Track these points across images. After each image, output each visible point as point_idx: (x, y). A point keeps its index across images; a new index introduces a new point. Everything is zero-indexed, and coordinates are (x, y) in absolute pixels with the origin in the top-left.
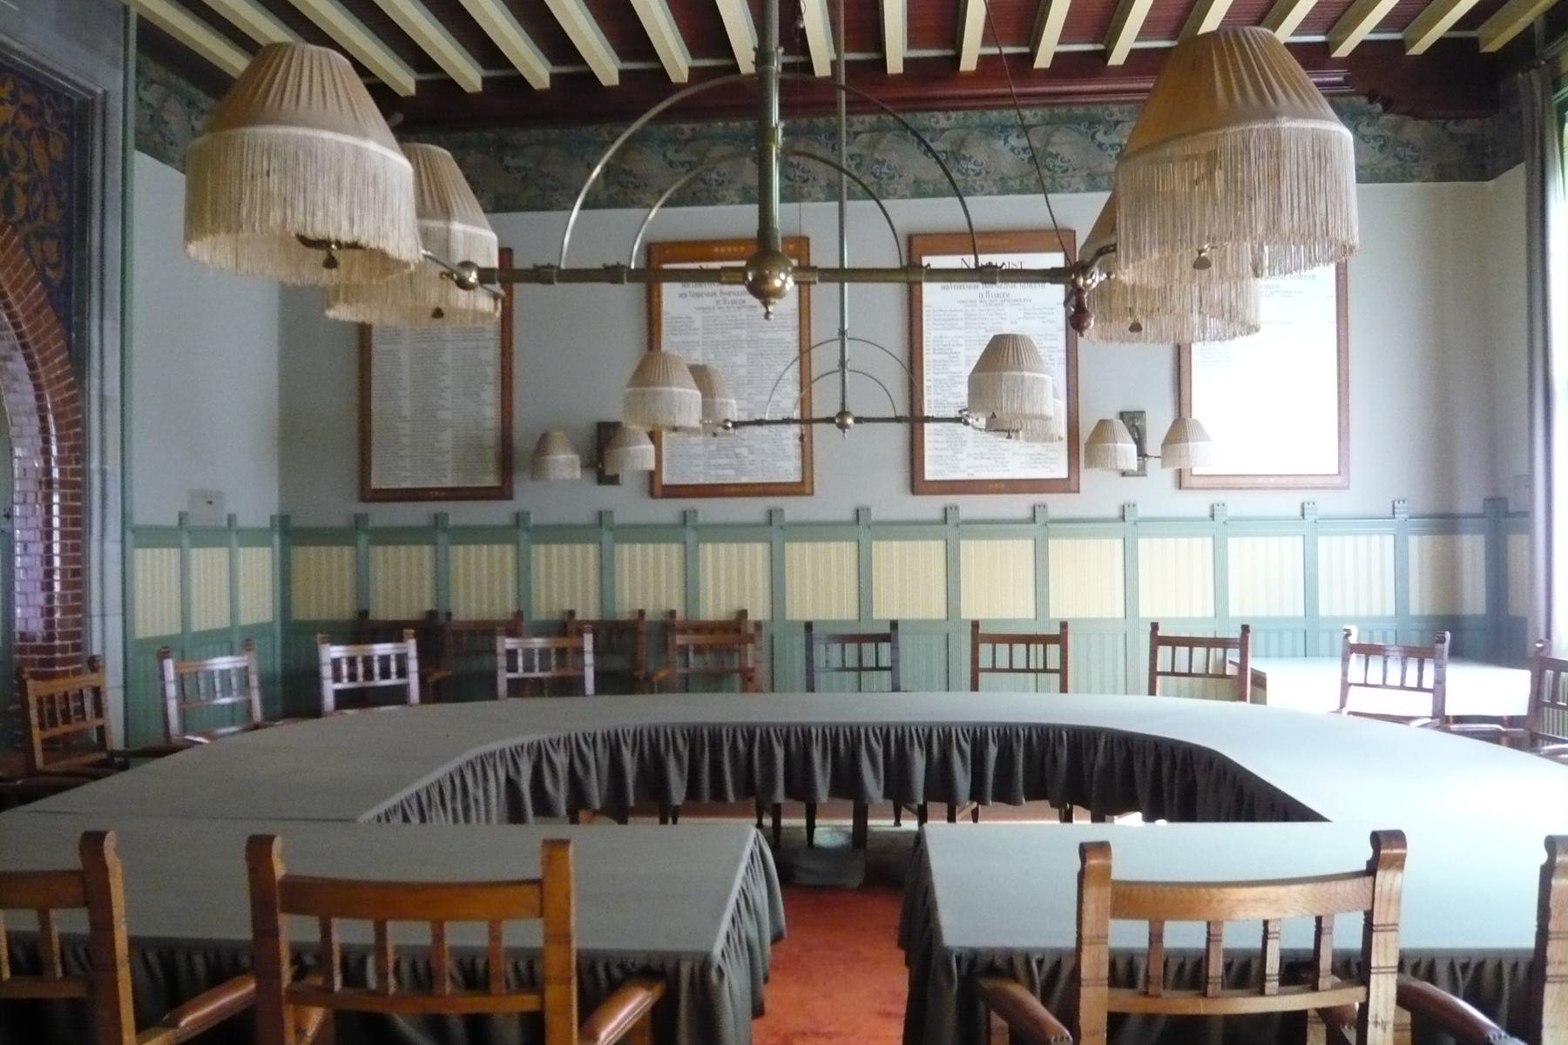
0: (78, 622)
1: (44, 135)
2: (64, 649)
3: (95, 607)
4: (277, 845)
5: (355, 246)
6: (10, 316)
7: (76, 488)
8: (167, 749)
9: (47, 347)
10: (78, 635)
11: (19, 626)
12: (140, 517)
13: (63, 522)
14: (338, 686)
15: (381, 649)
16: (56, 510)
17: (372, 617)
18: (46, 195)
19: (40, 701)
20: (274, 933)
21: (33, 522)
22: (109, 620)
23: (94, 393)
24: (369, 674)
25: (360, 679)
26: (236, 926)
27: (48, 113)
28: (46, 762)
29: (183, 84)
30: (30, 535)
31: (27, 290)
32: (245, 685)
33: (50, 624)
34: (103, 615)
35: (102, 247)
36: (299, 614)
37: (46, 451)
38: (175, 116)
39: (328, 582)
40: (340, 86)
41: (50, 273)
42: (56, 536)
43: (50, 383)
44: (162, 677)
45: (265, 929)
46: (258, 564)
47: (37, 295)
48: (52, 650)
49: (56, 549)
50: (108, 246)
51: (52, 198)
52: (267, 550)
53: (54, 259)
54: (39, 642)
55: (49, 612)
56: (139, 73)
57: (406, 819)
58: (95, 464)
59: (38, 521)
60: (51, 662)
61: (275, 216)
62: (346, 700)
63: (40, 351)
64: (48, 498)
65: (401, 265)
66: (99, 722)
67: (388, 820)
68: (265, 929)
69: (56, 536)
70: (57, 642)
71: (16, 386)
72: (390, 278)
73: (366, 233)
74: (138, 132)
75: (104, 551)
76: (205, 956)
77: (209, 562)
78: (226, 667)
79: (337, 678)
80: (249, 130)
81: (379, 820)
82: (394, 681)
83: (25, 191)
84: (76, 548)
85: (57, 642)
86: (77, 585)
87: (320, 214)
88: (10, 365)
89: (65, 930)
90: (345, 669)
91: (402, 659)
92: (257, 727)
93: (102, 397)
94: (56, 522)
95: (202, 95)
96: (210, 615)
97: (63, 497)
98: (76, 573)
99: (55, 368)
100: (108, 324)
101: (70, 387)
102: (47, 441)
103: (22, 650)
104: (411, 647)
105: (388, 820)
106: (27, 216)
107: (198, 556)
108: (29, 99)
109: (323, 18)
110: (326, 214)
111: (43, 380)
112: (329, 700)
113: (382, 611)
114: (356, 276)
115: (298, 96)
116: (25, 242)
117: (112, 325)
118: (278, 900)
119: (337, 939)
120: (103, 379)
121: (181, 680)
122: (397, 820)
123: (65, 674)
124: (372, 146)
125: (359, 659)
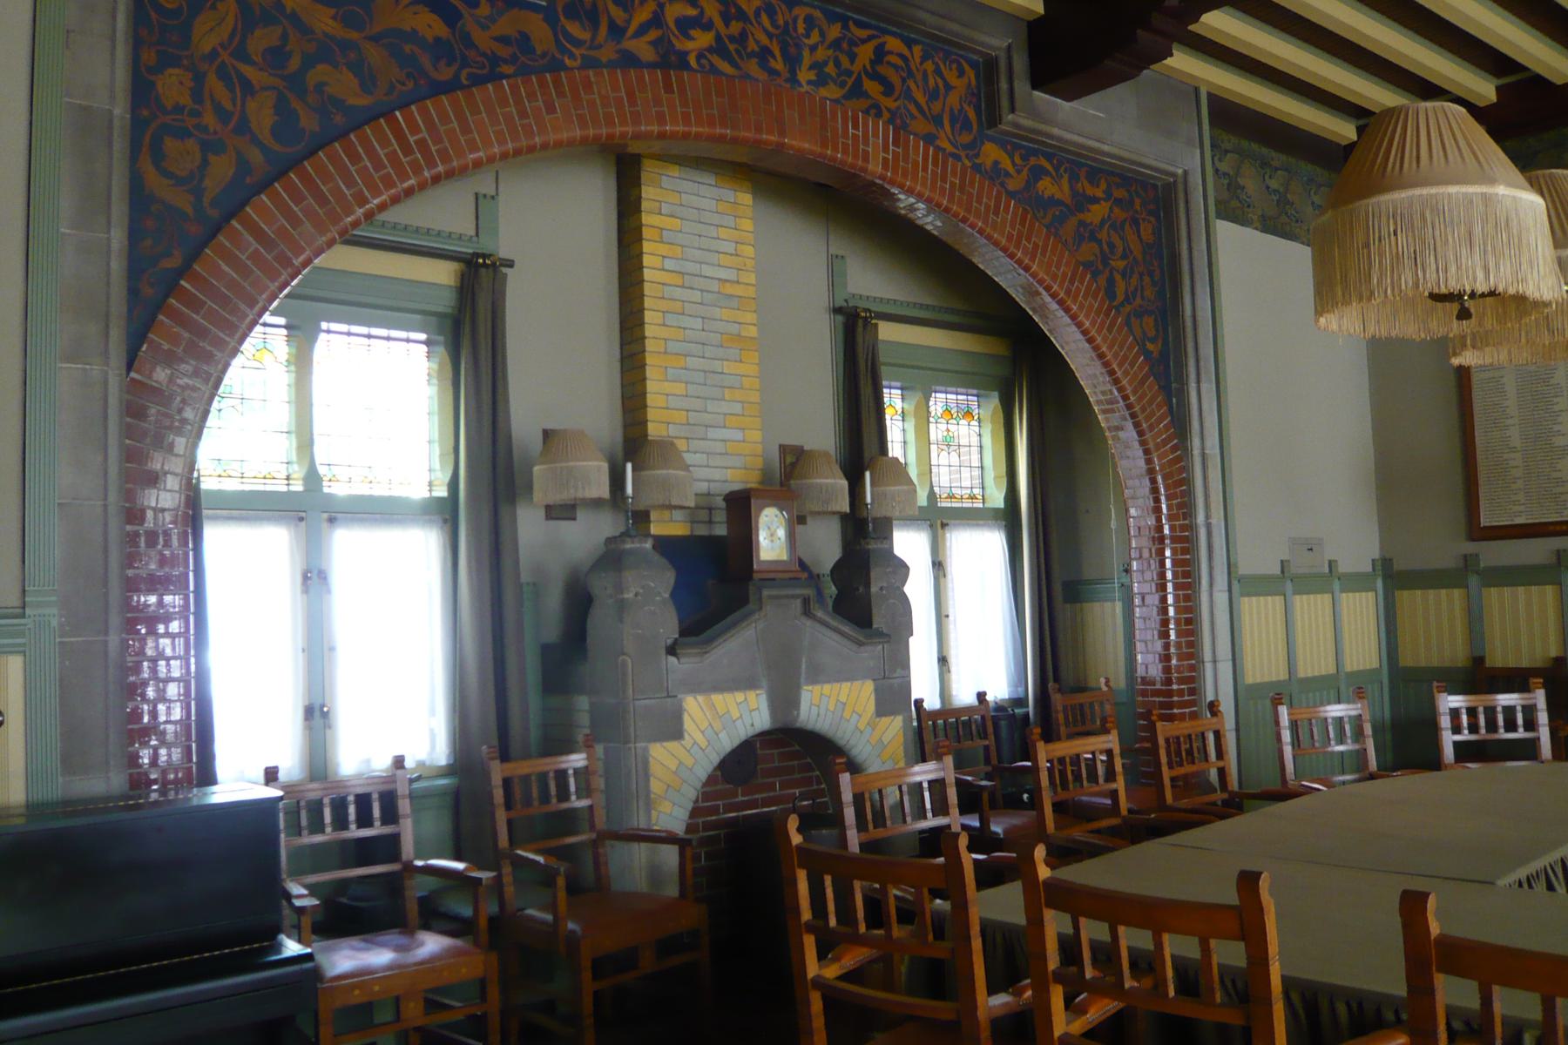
0: (1192, 668)
1: (1135, 222)
2: (1181, 693)
3: (1207, 656)
4: (1431, 903)
5: (1492, 294)
6: (1120, 390)
7: (1185, 542)
8: (1284, 794)
9: (1152, 414)
10: (1191, 680)
11: (1140, 671)
12: (1245, 568)
13: (1175, 575)
14: (1458, 738)
15: (1505, 699)
16: (1168, 563)
17: (1488, 664)
18: (1141, 275)
19: (1167, 741)
20: (1431, 992)
21: (1148, 575)
22: (1220, 666)
23: (1196, 452)
24: (1492, 726)
25: (1483, 731)
26: (1391, 982)
27: (1138, 202)
28: (1175, 799)
29: (1255, 146)
30: (1146, 588)
31: (1132, 365)
32: (1359, 734)
33: (1167, 670)
34: (1215, 661)
35: (1194, 317)
36: (1407, 660)
37: (1157, 510)
38: (1250, 183)
39: (1438, 625)
40: (1462, 143)
41: (1150, 346)
42: (1170, 587)
43: (1158, 447)
44: (1277, 723)
45: (1420, 987)
46: (1361, 610)
47: (1141, 368)
48: (1170, 693)
49: (1170, 599)
50: (1199, 314)
51: (1147, 279)
52: (1371, 595)
53: (1152, 333)
54: (1158, 686)
55: (1166, 658)
56: (1213, 146)
57: (1550, 887)
58: (1201, 518)
59: (1151, 574)
60: (1170, 706)
61: (1407, 279)
62: (1465, 752)
63: (1147, 419)
64: (1161, 553)
65: (1539, 305)
66: (1221, 764)
67: (1530, 886)
68: (1420, 987)
69: (1170, 587)
70: (1175, 687)
71: (1129, 453)
72: (1526, 320)
73: (1503, 279)
74: (1218, 203)
75: (1214, 600)
76: (1348, 1005)
77: (1312, 609)
78: (1339, 714)
79: (1457, 729)
80: (1374, 200)
81: (1520, 885)
82: (1521, 734)
83: (1124, 275)
84: (1187, 598)
85: (1175, 687)
86: (1191, 633)
87: (1453, 269)
88: (1121, 434)
89: (1223, 961)
90: (1464, 718)
91: (1529, 710)
92: (1372, 777)
93: (1203, 456)
94: (1169, 575)
95: (1273, 154)
96: (1315, 661)
97: (1174, 552)
98: (1189, 621)
99: (1159, 434)
100: (1204, 386)
101: (1174, 449)
102: (1157, 500)
103: (1144, 693)
104: (1540, 698)
105: (1530, 886)
106: (1127, 299)
107: (1300, 602)
108: (1119, 193)
109: (1375, 41)
110: (1459, 268)
111: (1151, 446)
112: (1448, 753)
113: (1500, 656)
114: (1490, 323)
115: (1418, 157)
116: (1127, 323)
117: (1208, 388)
118: (282, 825)
119: (1498, 1008)
120: (1204, 440)
121: (1294, 726)
122: (1541, 886)
123: (1182, 717)
124: (1501, 190)
125: (1481, 709)
